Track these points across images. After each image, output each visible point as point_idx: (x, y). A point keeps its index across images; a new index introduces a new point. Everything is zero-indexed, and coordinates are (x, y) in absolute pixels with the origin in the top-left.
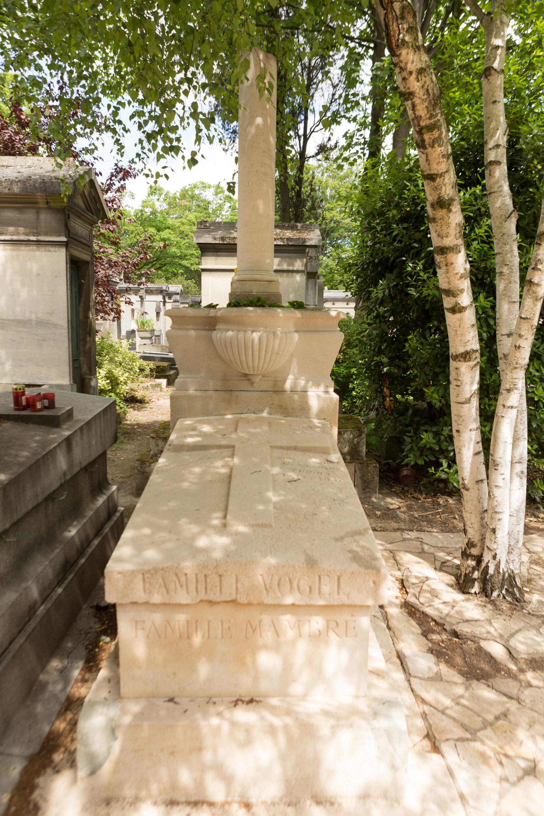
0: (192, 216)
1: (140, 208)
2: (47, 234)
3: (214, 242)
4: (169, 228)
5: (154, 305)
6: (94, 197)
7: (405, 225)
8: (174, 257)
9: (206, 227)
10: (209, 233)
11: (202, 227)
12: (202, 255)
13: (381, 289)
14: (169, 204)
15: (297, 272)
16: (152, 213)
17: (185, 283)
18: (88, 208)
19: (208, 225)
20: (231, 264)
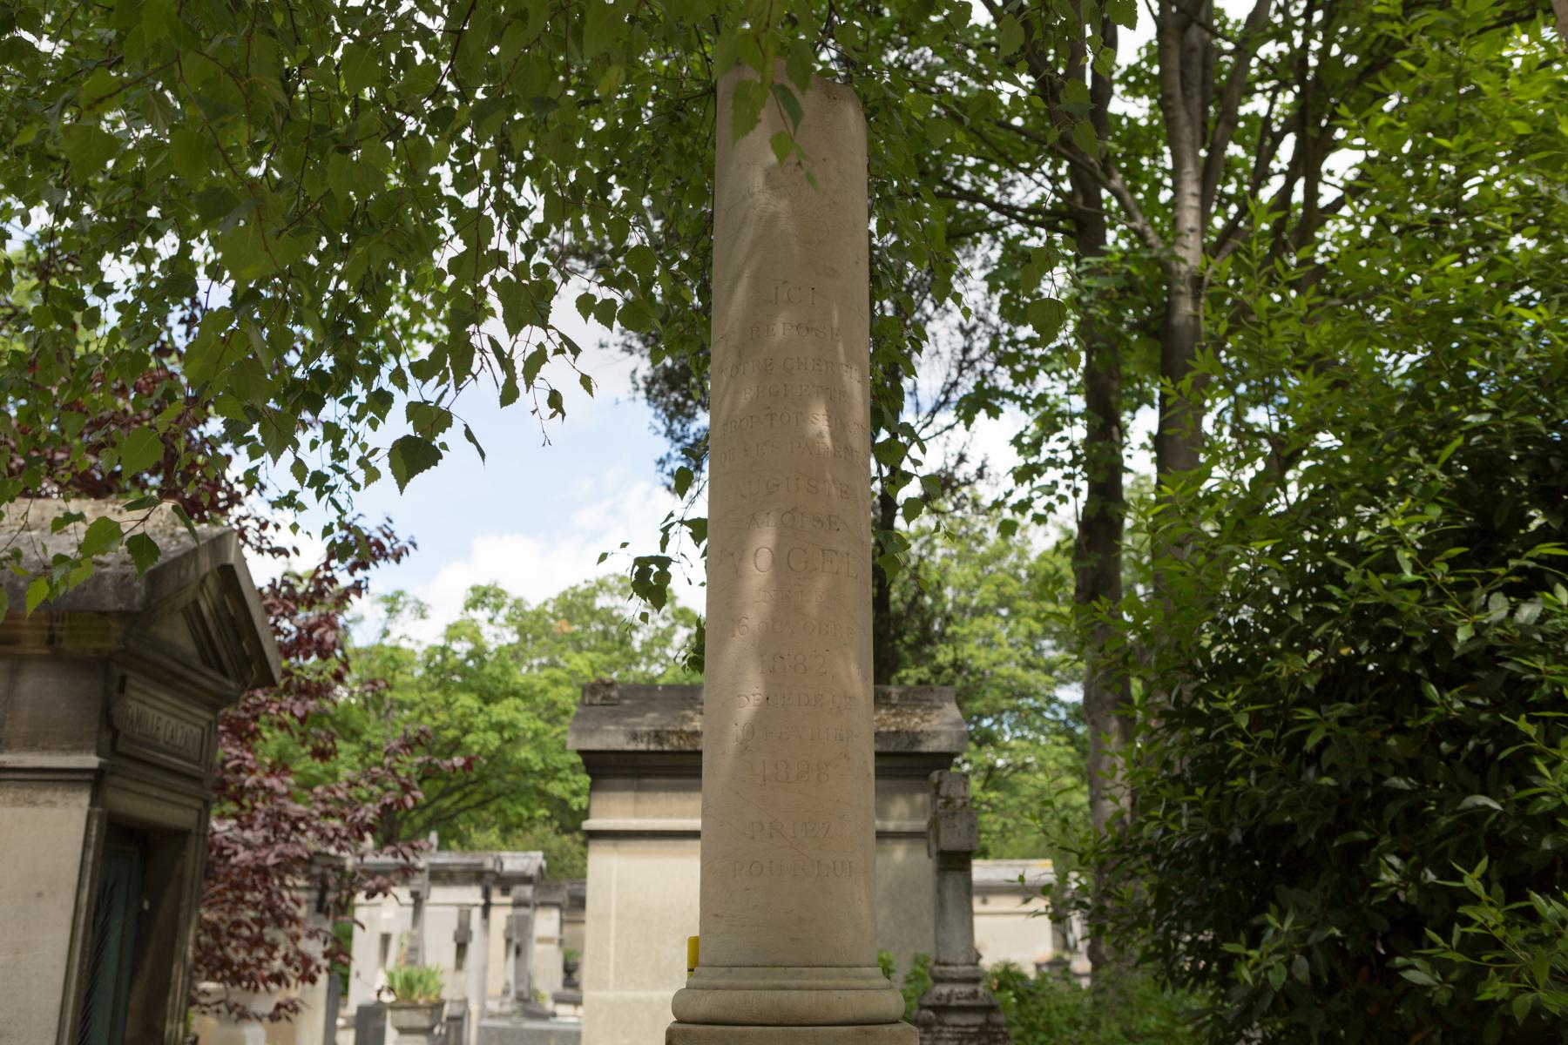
0: (580, 663)
1: (441, 642)
2: (32, 745)
3: (631, 747)
4: (515, 694)
5: (451, 921)
6: (232, 619)
7: (1346, 708)
8: (525, 770)
9: (608, 702)
10: (615, 717)
11: (598, 700)
12: (593, 787)
13: (1274, 955)
14: (521, 631)
15: (897, 836)
16: (471, 655)
17: (555, 842)
18: (210, 657)
19: (614, 694)
20: (682, 815)
